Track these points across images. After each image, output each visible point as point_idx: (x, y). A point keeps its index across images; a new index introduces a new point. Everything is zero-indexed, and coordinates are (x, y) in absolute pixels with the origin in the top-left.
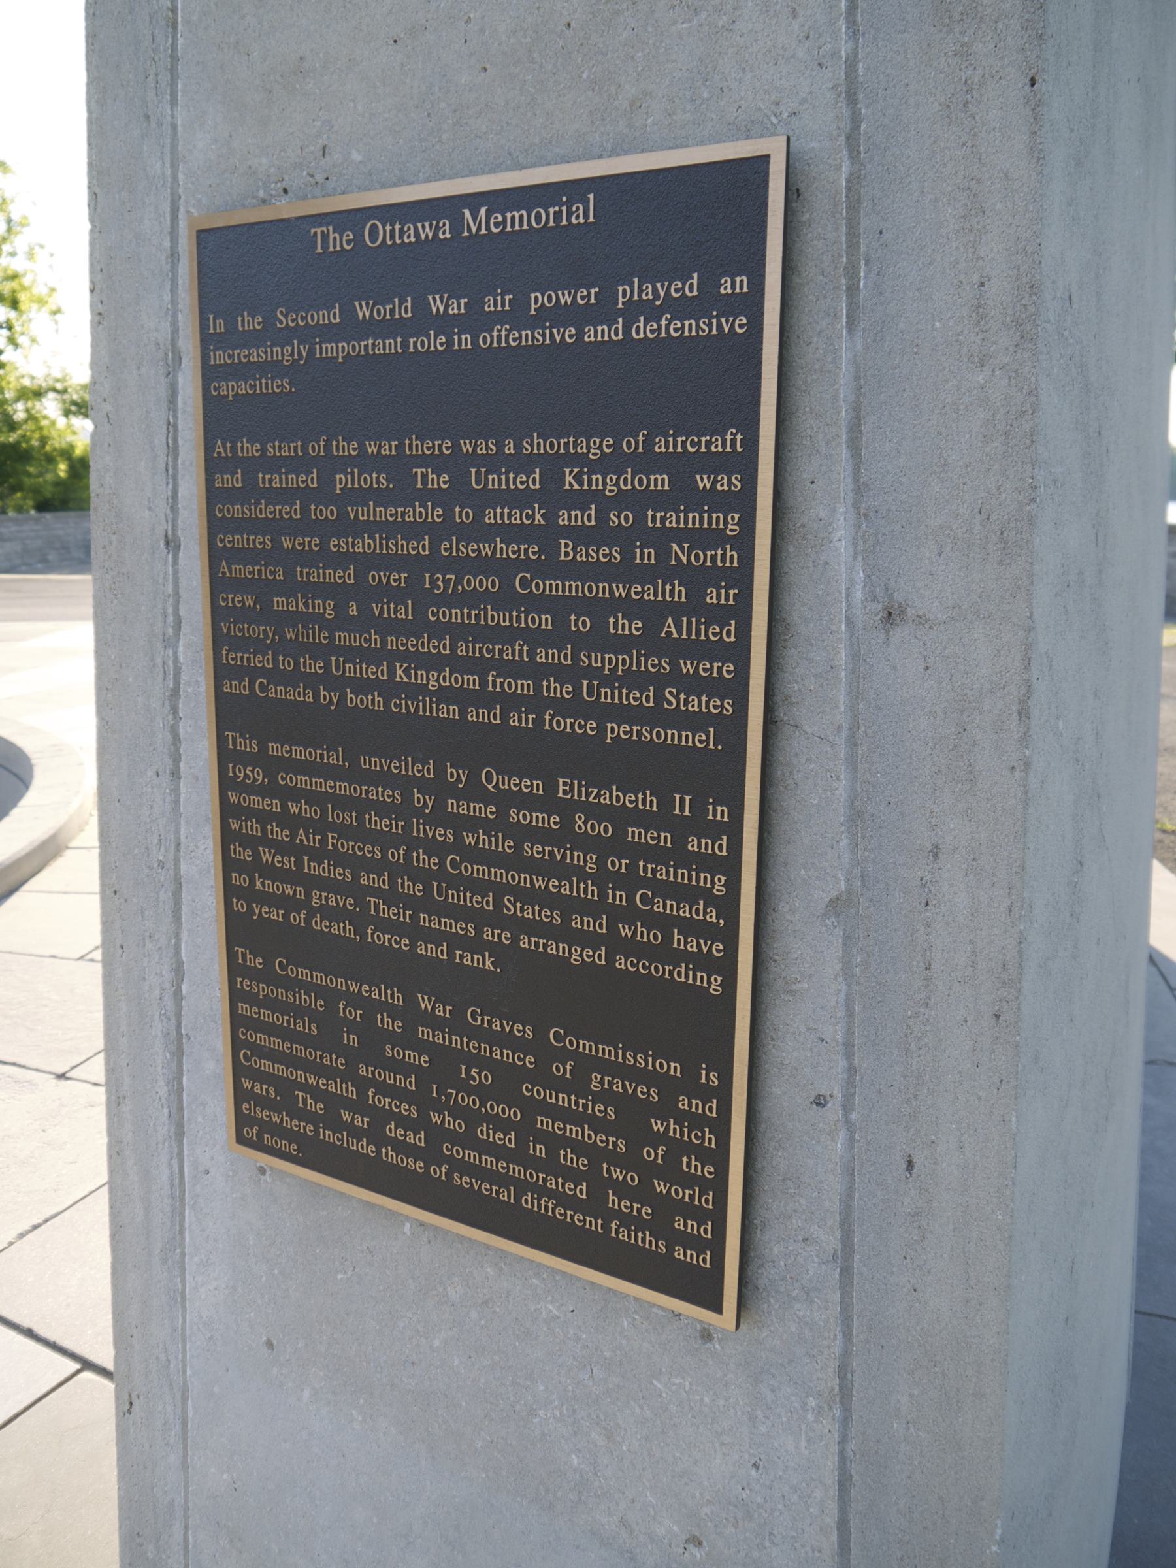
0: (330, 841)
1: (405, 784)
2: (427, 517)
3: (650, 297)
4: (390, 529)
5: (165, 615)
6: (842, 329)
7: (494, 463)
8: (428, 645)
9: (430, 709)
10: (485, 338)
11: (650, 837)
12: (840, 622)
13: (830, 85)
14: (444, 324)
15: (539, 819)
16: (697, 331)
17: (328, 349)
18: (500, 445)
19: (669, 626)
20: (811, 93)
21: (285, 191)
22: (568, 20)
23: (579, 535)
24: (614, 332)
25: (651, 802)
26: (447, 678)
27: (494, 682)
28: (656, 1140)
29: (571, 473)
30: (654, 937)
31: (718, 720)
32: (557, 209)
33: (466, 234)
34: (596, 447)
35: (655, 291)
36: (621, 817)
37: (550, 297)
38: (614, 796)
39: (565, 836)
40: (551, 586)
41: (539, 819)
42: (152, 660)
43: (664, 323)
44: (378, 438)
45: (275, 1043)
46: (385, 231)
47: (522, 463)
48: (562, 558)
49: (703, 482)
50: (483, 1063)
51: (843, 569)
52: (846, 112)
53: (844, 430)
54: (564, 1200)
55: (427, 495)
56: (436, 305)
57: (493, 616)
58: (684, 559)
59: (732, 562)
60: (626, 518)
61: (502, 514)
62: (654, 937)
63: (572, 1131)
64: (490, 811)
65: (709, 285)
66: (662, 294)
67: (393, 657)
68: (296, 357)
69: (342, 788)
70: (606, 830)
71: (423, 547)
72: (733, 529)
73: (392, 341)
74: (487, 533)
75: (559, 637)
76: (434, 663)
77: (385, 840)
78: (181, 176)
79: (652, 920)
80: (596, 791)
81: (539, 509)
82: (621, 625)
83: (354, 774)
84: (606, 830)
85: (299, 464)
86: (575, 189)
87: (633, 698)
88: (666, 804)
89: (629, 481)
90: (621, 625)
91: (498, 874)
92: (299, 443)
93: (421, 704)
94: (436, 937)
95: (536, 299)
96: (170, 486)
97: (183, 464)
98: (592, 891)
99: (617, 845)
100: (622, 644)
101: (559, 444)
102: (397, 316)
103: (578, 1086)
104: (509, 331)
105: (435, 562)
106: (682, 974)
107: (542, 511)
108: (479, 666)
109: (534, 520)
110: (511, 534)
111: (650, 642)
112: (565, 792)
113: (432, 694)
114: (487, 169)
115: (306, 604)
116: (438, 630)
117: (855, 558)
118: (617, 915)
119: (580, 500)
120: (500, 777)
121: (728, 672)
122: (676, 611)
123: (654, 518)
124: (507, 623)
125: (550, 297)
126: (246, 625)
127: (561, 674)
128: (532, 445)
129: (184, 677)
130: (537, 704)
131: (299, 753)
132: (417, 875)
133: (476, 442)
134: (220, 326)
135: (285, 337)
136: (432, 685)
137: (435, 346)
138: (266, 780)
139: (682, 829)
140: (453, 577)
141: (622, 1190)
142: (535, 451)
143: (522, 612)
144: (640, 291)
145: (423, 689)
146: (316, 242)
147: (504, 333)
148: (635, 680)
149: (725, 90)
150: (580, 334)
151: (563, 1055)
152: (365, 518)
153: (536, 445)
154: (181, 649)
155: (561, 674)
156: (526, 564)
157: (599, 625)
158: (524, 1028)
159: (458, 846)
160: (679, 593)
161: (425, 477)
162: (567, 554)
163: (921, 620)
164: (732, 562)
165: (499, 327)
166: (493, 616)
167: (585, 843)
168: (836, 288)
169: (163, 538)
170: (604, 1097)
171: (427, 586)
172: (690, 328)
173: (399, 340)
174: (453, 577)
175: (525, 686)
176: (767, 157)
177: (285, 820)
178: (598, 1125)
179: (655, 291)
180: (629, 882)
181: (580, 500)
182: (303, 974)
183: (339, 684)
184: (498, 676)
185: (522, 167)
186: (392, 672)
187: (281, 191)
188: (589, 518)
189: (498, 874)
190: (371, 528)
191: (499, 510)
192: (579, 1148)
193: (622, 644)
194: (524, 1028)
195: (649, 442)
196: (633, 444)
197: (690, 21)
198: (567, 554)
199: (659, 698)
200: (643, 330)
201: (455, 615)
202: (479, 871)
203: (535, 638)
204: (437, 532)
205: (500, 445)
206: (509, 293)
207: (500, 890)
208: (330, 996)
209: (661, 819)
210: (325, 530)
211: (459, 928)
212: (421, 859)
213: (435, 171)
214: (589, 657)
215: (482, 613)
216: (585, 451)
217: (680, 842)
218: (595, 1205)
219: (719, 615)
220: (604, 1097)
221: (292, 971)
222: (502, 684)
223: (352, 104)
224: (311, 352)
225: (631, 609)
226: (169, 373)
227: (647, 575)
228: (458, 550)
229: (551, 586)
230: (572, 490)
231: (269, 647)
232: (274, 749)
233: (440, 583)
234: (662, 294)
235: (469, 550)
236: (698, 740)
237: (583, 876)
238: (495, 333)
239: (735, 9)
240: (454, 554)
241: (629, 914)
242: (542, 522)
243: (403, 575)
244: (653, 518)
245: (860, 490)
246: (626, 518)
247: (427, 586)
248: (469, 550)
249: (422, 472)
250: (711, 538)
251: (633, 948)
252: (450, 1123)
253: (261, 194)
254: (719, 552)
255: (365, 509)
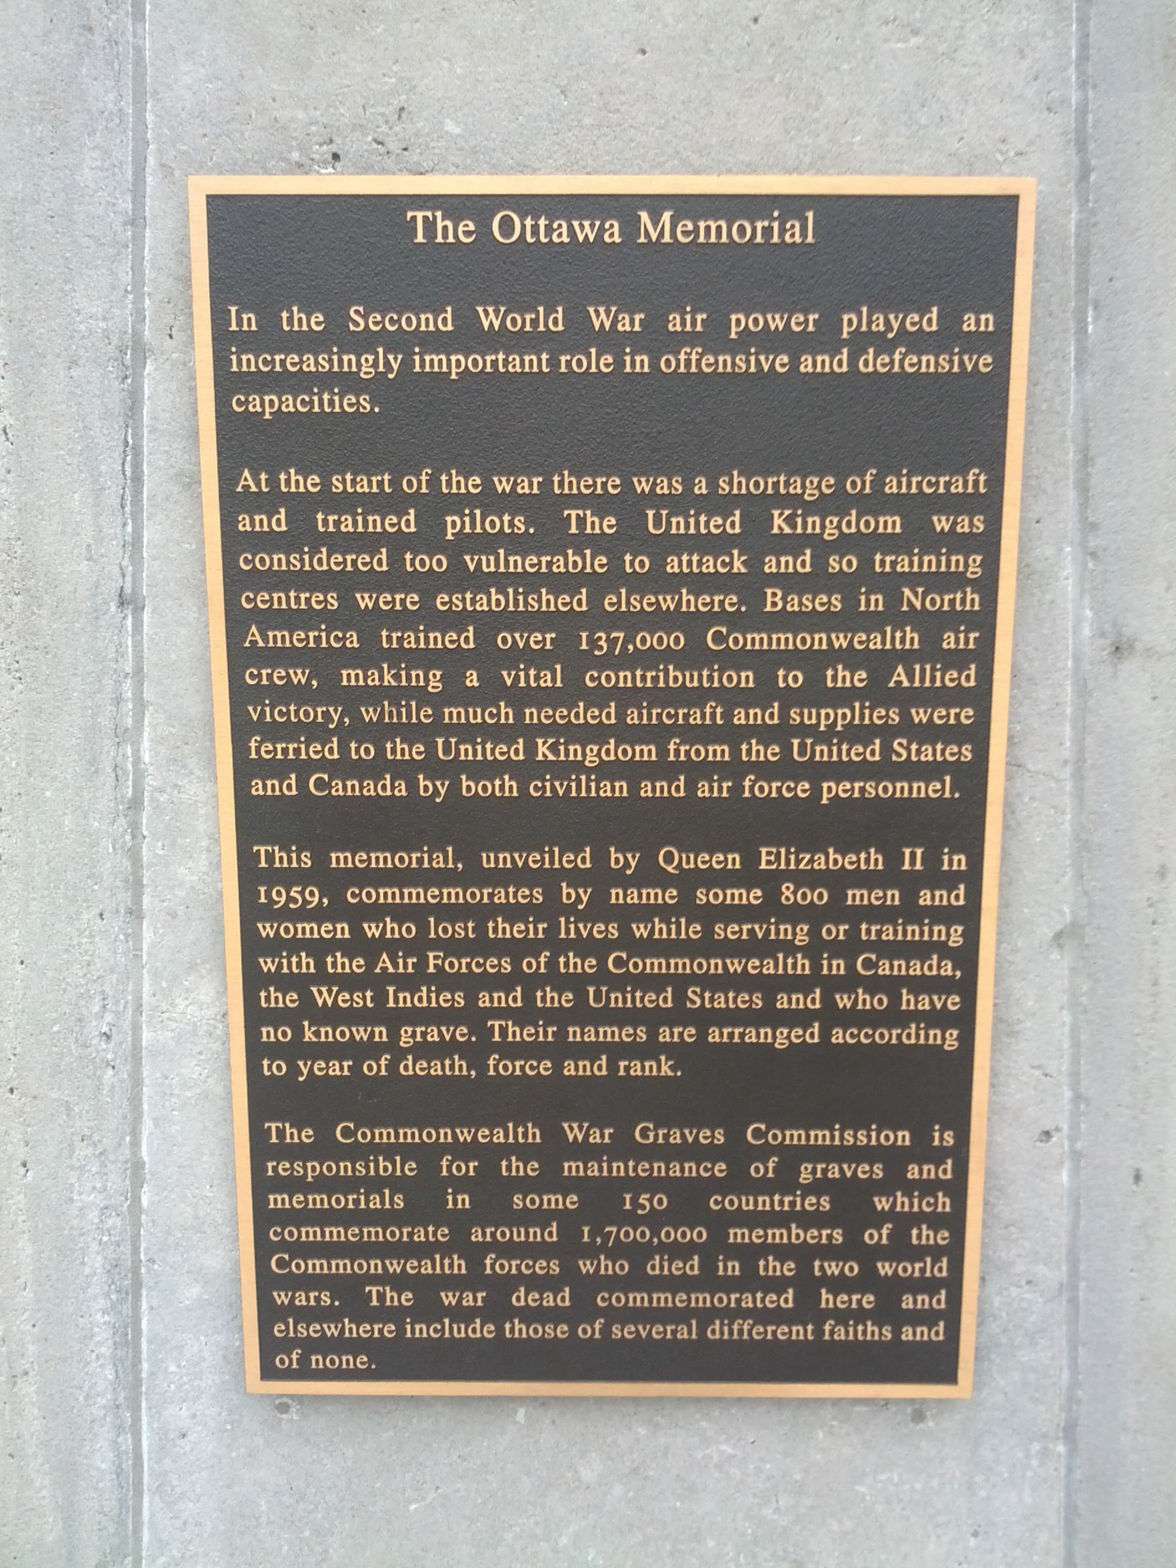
0: (432, 962)
1: (549, 879)
2: (584, 567)
3: (882, 328)
4: (531, 582)
5: (118, 701)
6: (1070, 372)
7: (678, 504)
8: (583, 714)
9: (584, 788)
10: (668, 361)
11: (875, 897)
12: (1067, 658)
13: (1060, 130)
14: (611, 341)
15: (736, 896)
16: (936, 368)
17: (434, 362)
18: (688, 484)
19: (899, 675)
20: (1039, 136)
21: (336, 157)
22: (756, 14)
23: (790, 583)
24: (841, 363)
25: (875, 860)
26: (612, 751)
27: (677, 752)
28: (879, 1218)
29: (781, 515)
30: (880, 1002)
31: (956, 768)
32: (766, 224)
33: (642, 240)
34: (812, 488)
35: (887, 322)
36: (838, 881)
37: (756, 321)
38: (831, 859)
39: (771, 908)
40: (756, 640)
41: (736, 896)
42: (93, 762)
43: (897, 357)
44: (512, 471)
45: (334, 1233)
46: (523, 227)
47: (719, 505)
48: (768, 608)
49: (941, 523)
50: (652, 1185)
51: (1070, 606)
52: (1075, 159)
53: (1071, 471)
54: (763, 1316)
55: (581, 542)
56: (600, 318)
57: (675, 677)
58: (918, 605)
59: (972, 605)
60: (850, 563)
61: (690, 563)
62: (880, 1002)
63: (777, 1235)
64: (671, 896)
65: (952, 320)
66: (896, 326)
67: (532, 733)
68: (381, 369)
69: (453, 895)
70: (819, 896)
71: (581, 602)
72: (974, 569)
73: (534, 358)
74: (674, 583)
75: (763, 694)
76: (596, 734)
77: (517, 949)
78: (149, 117)
79: (874, 985)
80: (808, 857)
81: (739, 556)
82: (840, 677)
83: (474, 876)
84: (819, 896)
85: (393, 503)
86: (792, 205)
87: (855, 753)
88: (893, 859)
89: (853, 523)
90: (840, 677)
91: (680, 965)
92: (387, 477)
93: (573, 784)
94: (590, 1051)
95: (738, 321)
96: (129, 529)
97: (152, 497)
98: (803, 966)
99: (836, 911)
100: (844, 697)
101: (766, 483)
102: (542, 328)
103: (786, 1182)
104: (702, 355)
105: (597, 618)
106: (912, 1035)
107: (743, 558)
108: (658, 734)
109: (732, 568)
110: (700, 583)
111: (877, 693)
112: (769, 862)
113: (589, 771)
114: (645, 166)
115: (397, 677)
116: (599, 697)
117: (1082, 592)
118: (832, 985)
119: (792, 545)
120: (684, 856)
121: (413, 603)
122: (907, 658)
123: (883, 563)
124: (696, 684)
125: (756, 321)
126: (292, 708)
127: (765, 734)
128: (731, 483)
129: (150, 782)
130: (735, 770)
131: (381, 859)
132: (561, 982)
133: (655, 480)
134: (250, 320)
135: (365, 342)
136: (591, 760)
137: (598, 366)
138: (325, 901)
139: (911, 884)
140: (622, 635)
141: (839, 1285)
142: (735, 491)
143: (714, 671)
144: (870, 323)
145: (579, 767)
146: (416, 229)
147: (694, 357)
148: (857, 734)
149: (946, 120)
150: (795, 363)
151: (763, 1153)
152: (492, 569)
153: (736, 483)
154: (146, 744)
155: (765, 734)
156: (722, 617)
157: (815, 680)
158: (713, 1133)
159: (628, 942)
160: (911, 638)
161: (581, 521)
162: (774, 604)
163: (1149, 652)
164: (972, 605)
165: (688, 350)
166: (675, 677)
167: (794, 914)
168: (1064, 331)
169: (117, 598)
170: (818, 1187)
171: (584, 647)
172: (928, 363)
173: (544, 357)
174: (622, 635)
175: (719, 752)
176: (1014, 199)
177: (357, 946)
178: (808, 1220)
179: (887, 322)
180: (849, 948)
181: (792, 545)
182: (384, 1135)
183: (452, 770)
184: (682, 743)
185: (697, 172)
186: (531, 749)
187: (329, 157)
188: (805, 563)
189: (680, 965)
190: (502, 581)
191: (685, 558)
192: (782, 1252)
193: (844, 697)
194: (713, 1133)
195: (878, 482)
196: (861, 483)
197: (906, 40)
198: (774, 604)
199: (887, 749)
200: (872, 362)
201: (625, 680)
202: (654, 965)
203: (732, 698)
204: (599, 585)
205: (688, 484)
206: (701, 310)
207: (681, 983)
208: (427, 1155)
209: (891, 876)
210: (429, 584)
211: (625, 1034)
212: (571, 963)
213: (573, 159)
214: (801, 715)
215: (661, 674)
216: (799, 491)
217: (910, 897)
218: (807, 1311)
219: (958, 660)
220: (818, 1187)
221: (364, 1136)
222: (687, 753)
223: (446, 64)
224: (407, 364)
225: (851, 658)
226: (126, 377)
227: (874, 622)
228: (628, 603)
229: (756, 640)
230: (782, 535)
231: (333, 732)
232: (339, 859)
233: (603, 643)
234: (896, 326)
235: (646, 603)
236: (933, 790)
237: (789, 948)
238: (682, 357)
239: (957, 38)
240: (624, 608)
241: (850, 982)
242: (743, 570)
243: (548, 636)
244: (882, 562)
245: (1089, 527)
246: (850, 563)
247: (584, 647)
248: (646, 603)
249: (578, 515)
250: (952, 581)
251: (853, 1018)
252: (607, 1267)
253: (295, 155)
254: (959, 596)
255: (492, 558)
